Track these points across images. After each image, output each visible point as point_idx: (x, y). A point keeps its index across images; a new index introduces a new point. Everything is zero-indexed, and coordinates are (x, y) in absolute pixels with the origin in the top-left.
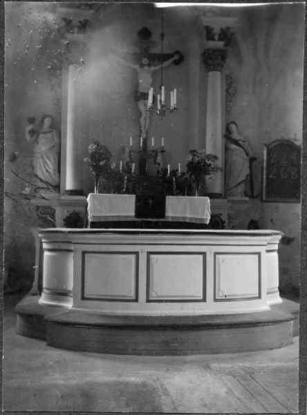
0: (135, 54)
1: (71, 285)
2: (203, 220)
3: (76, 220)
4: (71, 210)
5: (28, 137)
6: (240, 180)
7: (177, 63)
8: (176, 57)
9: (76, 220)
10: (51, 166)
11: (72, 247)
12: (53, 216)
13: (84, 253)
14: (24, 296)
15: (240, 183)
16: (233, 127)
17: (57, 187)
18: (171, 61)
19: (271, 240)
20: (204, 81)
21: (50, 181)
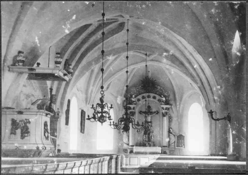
0: (143, 75)
1: (128, 164)
2: (159, 152)
3: (131, 152)
4: (131, 150)
5: (122, 132)
6: (172, 143)
7: (157, 114)
8: (157, 112)
9: (131, 152)
10: (127, 140)
11: (128, 157)
12: (127, 151)
13: (130, 158)
14: (171, 164)
15: (173, 143)
16: (171, 129)
17: (128, 144)
18: (155, 113)
19: (100, 166)
20: (163, 118)
21: (126, 143)
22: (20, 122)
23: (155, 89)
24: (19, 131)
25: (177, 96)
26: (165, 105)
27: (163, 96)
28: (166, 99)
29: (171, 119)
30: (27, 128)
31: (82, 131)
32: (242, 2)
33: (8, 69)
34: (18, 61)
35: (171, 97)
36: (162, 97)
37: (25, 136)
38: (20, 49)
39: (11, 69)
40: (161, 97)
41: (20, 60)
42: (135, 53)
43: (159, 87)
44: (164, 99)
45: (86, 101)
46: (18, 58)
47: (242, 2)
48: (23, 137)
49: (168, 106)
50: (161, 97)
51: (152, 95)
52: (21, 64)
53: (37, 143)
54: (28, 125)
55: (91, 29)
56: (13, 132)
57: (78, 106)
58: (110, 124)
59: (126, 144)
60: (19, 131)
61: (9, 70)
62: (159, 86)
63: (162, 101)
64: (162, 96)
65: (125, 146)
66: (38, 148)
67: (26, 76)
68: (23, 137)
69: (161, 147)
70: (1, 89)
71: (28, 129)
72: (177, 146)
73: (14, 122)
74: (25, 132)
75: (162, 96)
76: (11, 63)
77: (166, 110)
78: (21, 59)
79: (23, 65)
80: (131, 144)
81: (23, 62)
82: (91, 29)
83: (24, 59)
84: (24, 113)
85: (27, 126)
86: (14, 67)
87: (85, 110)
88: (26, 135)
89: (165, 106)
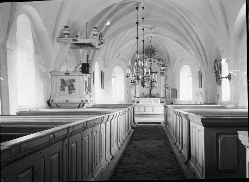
5: (130, 88)
10: (134, 93)
12: (134, 102)
16: (166, 85)
17: (135, 97)
22: (67, 81)
23: (155, 55)
24: (67, 88)
25: (171, 61)
26: (162, 67)
27: (161, 60)
28: (163, 63)
29: (166, 77)
30: (73, 86)
31: (103, 88)
32: (248, 150)
33: (57, 40)
34: (64, 34)
35: (167, 61)
36: (160, 61)
37: (72, 92)
38: (65, 25)
39: (59, 40)
40: (159, 61)
41: (66, 33)
42: (125, 17)
43: (158, 54)
44: (161, 63)
45: (105, 65)
46: (65, 32)
47: (248, 150)
48: (70, 93)
49: (164, 68)
50: (159, 61)
51: (153, 60)
52: (66, 36)
53: (81, 97)
54: (73, 83)
55: (114, 8)
56: (63, 89)
57: (99, 68)
58: (131, 82)
59: (133, 96)
60: (67, 88)
61: (58, 41)
62: (157, 52)
63: (160, 64)
64: (160, 60)
65: (133, 98)
66: (82, 101)
67: (69, 45)
68: (70, 93)
69: (160, 98)
70: (248, 78)
71: (74, 86)
72: (171, 97)
73: (62, 80)
74: (72, 89)
75: (160, 60)
76: (59, 36)
77: (163, 71)
78: (67, 32)
79: (68, 37)
80: (137, 96)
81: (68, 34)
82: (114, 8)
83: (68, 32)
84: (70, 75)
85: (72, 84)
86: (61, 38)
87: (103, 72)
88: (72, 91)
89: (162, 68)
